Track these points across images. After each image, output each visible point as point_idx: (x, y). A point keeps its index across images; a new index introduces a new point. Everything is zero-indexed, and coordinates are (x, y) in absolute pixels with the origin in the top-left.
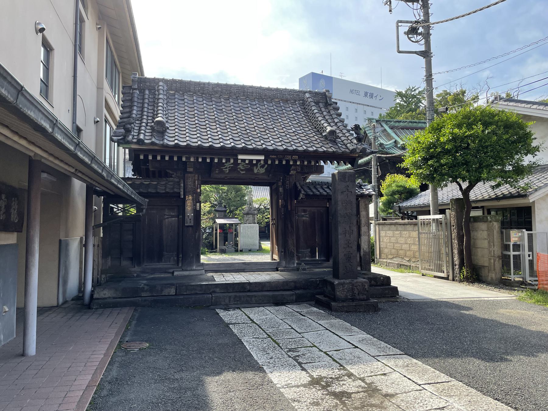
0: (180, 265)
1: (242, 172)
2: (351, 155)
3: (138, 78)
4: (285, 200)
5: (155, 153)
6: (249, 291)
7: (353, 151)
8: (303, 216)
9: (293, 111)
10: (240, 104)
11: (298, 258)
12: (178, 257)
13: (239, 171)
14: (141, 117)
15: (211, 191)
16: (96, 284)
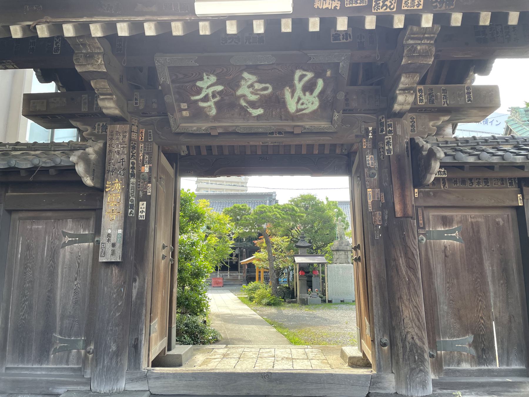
4: (385, 190)
8: (441, 236)
11: (438, 365)
15: (284, 218)
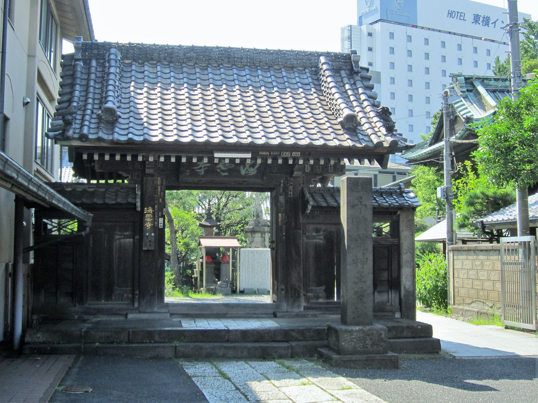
0: (136, 305)
1: (224, 174)
2: (376, 151)
3: (83, 44)
5: (102, 151)
6: (228, 341)
7: (380, 144)
8: (314, 237)
9: (299, 85)
10: (223, 76)
11: (307, 299)
12: (133, 294)
13: (218, 173)
14: (86, 96)
16: (27, 325)
